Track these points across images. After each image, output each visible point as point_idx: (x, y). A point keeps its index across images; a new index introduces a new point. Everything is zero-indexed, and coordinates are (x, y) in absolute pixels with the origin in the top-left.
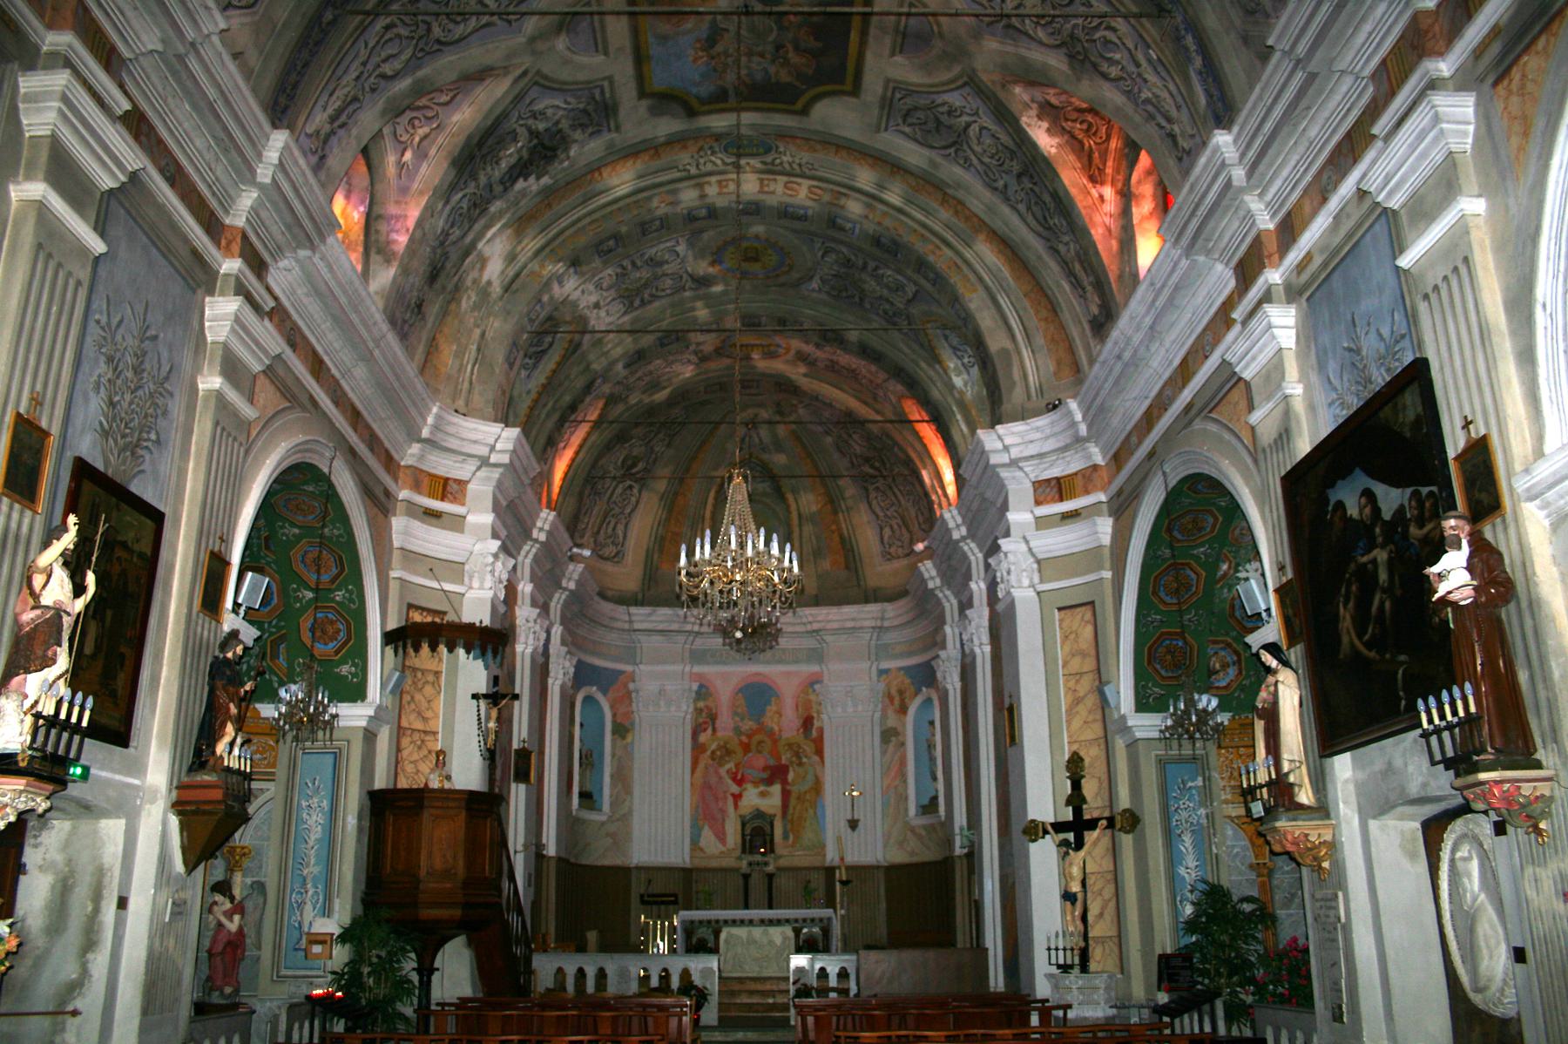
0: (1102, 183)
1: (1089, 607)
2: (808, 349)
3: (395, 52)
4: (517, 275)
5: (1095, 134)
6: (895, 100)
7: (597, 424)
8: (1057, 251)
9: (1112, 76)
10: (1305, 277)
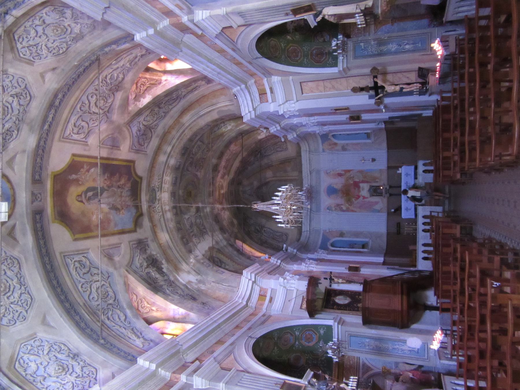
0: (161, 80)
1: (303, 84)
2: (220, 175)
3: (117, 316)
4: (195, 271)
5: (145, 83)
6: (136, 149)
7: (244, 242)
8: (185, 95)
9: (122, 76)
10: (184, 7)
